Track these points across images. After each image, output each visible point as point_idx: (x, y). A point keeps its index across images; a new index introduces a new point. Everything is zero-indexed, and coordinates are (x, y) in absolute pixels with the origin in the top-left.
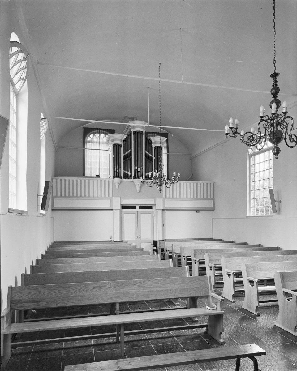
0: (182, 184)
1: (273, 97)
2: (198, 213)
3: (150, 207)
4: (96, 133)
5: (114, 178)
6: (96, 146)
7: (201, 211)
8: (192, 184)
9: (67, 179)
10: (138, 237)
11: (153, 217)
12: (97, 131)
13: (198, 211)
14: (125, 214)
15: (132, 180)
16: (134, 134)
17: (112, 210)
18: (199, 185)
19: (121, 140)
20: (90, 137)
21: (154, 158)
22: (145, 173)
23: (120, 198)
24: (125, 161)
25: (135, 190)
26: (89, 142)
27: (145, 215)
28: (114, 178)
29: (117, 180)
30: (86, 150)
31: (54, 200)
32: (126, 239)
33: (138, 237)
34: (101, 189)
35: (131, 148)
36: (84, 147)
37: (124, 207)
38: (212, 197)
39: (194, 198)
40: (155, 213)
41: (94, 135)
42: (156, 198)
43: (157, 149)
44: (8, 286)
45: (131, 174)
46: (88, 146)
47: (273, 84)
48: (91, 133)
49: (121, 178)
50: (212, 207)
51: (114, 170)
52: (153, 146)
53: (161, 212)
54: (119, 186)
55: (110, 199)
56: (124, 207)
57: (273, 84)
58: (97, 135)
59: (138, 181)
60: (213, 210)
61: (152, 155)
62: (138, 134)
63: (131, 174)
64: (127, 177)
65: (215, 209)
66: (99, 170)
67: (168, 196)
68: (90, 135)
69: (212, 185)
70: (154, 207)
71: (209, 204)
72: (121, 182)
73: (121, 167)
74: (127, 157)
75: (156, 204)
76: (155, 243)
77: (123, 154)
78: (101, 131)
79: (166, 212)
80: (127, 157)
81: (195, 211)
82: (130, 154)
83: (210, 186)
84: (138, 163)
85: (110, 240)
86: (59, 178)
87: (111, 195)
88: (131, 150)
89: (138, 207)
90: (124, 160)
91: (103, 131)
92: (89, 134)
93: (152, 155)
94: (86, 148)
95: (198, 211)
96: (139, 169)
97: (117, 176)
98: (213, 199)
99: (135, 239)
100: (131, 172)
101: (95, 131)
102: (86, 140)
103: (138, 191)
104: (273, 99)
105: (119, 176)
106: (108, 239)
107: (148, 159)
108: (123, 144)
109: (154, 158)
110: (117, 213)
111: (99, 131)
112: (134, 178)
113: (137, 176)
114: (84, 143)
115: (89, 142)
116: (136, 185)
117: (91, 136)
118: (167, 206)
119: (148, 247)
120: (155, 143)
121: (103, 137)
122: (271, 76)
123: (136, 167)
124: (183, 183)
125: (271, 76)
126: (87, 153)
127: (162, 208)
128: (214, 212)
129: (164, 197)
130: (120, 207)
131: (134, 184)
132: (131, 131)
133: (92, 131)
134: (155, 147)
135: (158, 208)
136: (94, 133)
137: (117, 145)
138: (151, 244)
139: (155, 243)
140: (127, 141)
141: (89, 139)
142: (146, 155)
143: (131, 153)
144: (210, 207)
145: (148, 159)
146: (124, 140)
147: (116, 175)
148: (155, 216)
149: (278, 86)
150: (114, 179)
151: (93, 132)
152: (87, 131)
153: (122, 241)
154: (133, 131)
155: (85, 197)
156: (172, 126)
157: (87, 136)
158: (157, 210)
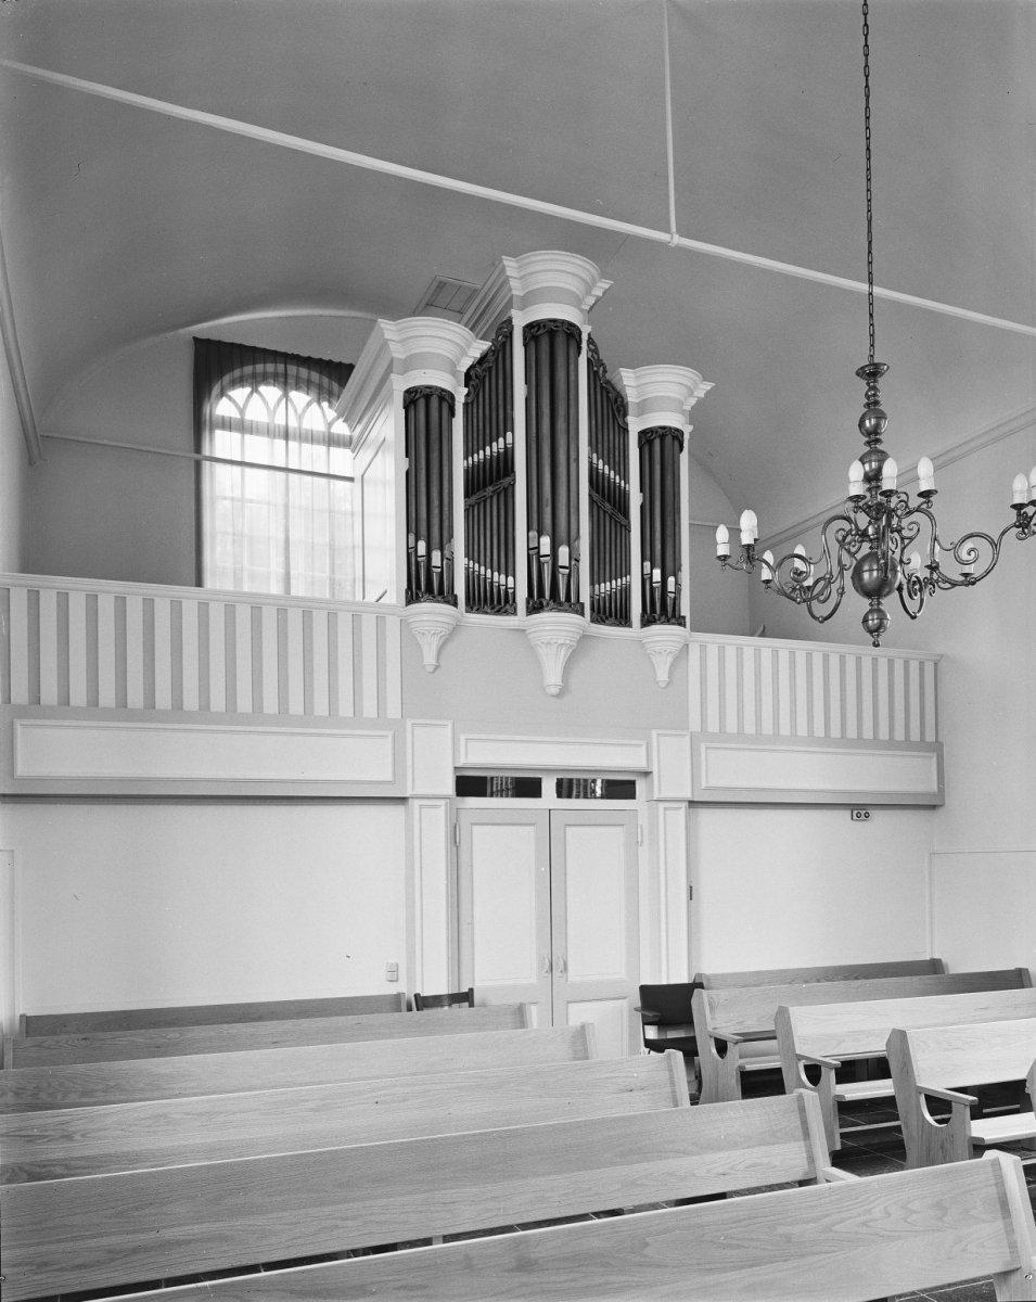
0: (713, 651)
1: (868, 443)
2: (860, 826)
3: (620, 789)
4: (264, 378)
5: (412, 596)
6: (258, 448)
7: (874, 813)
8: (784, 656)
9: (108, 590)
10: (553, 966)
11: (633, 845)
12: (270, 367)
13: (860, 810)
14: (475, 828)
15: (520, 618)
16: (525, 345)
17: (403, 800)
18: (821, 661)
19: (452, 369)
20: (230, 398)
21: (635, 500)
22: (592, 583)
23: (448, 731)
24: (473, 499)
25: (543, 679)
26: (227, 425)
27: (594, 836)
28: (412, 596)
29: (431, 613)
30: (206, 465)
31: (19, 730)
32: (481, 980)
33: (553, 966)
34: (776, 691)
35: (508, 425)
36: (198, 448)
37: (470, 785)
38: (930, 738)
39: (827, 740)
40: (643, 820)
41: (255, 390)
42: (654, 733)
43: (657, 442)
45: (511, 584)
46: (222, 443)
48: (237, 373)
49: (455, 604)
50: (934, 788)
51: (411, 553)
52: (635, 425)
53: (682, 812)
55: (390, 734)
56: (470, 785)
58: (271, 392)
59: (556, 626)
60: (934, 807)
61: (626, 478)
62: (552, 339)
64: (488, 600)
65: (951, 800)
66: (282, 559)
67: (713, 727)
68: (234, 384)
69: (929, 667)
70: (640, 787)
71: (912, 775)
72: (456, 628)
74: (490, 480)
75: (655, 770)
76: (668, 1009)
77: (466, 458)
78: (292, 369)
79: (705, 815)
80: (490, 480)
81: (847, 813)
82: (505, 462)
83: (843, 671)
84: (550, 517)
85: (392, 990)
86: (50, 587)
87: (393, 711)
88: (509, 440)
89: (548, 787)
90: (467, 495)
91: (304, 372)
92: (227, 378)
93: (627, 481)
94: (206, 452)
95: (860, 810)
97: (429, 589)
98: (937, 748)
99: (534, 980)
100: (509, 570)
101: (260, 367)
102: (207, 409)
104: (868, 449)
105: (441, 592)
106: (375, 985)
107: (609, 500)
108: (461, 394)
109: (635, 500)
110: (433, 823)
111: (281, 367)
112: (534, 608)
113: (548, 595)
114: (199, 425)
115: (227, 425)
116: (542, 651)
117: (240, 393)
118: (713, 783)
119: (616, 1026)
120: (643, 407)
122: (861, 373)
123: (546, 541)
124: (722, 649)
125: (861, 373)
127: (688, 795)
128: (940, 811)
129: (695, 726)
130: (449, 787)
131: (531, 649)
132: (510, 321)
133: (242, 365)
134: (646, 437)
135: (666, 794)
136: (255, 381)
137: (428, 397)
138: (624, 1003)
139: (668, 1009)
140: (487, 376)
141: (223, 408)
142: (596, 479)
143: (507, 457)
144: (921, 788)
145: (609, 500)
146: (467, 375)
147: (423, 584)
148: (646, 842)
150: (415, 607)
151: (248, 369)
152: (218, 363)
153: (466, 997)
154: (520, 320)
155: (231, 715)
156: (825, 271)
157: (216, 390)
158: (662, 806)
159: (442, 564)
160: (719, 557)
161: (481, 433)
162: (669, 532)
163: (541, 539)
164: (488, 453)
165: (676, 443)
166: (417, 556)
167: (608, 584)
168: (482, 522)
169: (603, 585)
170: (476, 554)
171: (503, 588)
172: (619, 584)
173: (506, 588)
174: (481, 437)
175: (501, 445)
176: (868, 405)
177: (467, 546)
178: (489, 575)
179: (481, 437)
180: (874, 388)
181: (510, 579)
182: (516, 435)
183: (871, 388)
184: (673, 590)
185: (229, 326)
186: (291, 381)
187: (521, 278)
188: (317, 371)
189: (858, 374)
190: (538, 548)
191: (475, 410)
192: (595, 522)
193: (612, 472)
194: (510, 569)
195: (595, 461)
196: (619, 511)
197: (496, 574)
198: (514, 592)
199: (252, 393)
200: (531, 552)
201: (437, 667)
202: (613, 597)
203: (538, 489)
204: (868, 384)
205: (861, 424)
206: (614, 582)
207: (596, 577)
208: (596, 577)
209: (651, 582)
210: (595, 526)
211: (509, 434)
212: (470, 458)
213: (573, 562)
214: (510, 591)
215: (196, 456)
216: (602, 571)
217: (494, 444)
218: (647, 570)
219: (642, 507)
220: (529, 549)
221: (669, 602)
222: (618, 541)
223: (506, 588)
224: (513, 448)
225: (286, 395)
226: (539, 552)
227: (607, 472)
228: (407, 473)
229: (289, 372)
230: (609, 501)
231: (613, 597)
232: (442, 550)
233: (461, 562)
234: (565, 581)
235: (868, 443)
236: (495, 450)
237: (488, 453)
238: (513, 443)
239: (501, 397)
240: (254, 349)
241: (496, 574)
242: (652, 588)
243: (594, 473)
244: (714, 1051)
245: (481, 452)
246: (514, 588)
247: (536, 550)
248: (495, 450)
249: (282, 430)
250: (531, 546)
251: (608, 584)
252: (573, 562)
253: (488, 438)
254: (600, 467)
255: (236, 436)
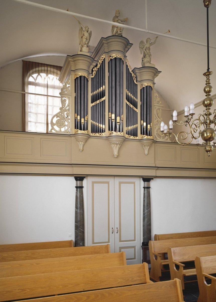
1: (206, 96)
4: (42, 71)
12: (43, 68)
20: (33, 77)
26: (31, 83)
41: (39, 74)
44: (212, 115)
45: (104, 127)
46: (31, 89)
47: (206, 83)
48: (34, 70)
54: (85, 146)
57: (206, 83)
58: (43, 75)
61: (137, 97)
63: (104, 127)
73: (87, 114)
78: (49, 69)
88: (104, 88)
91: (52, 69)
92: (31, 71)
94: (26, 92)
96: (118, 118)
100: (103, 123)
101: (40, 68)
103: (116, 156)
104: (206, 97)
111: (46, 68)
114: (24, 85)
115: (31, 83)
117: (35, 75)
121: (52, 79)
122: (204, 74)
123: (113, 116)
125: (204, 74)
126: (30, 99)
133: (36, 68)
136: (39, 72)
141: (31, 79)
149: (210, 85)
151: (37, 69)
152: (29, 67)
159: (84, 122)
160: (161, 131)
161: (96, 86)
162: (148, 112)
163: (112, 115)
164: (98, 91)
165: (151, 88)
166: (77, 120)
167: (131, 127)
168: (96, 110)
169: (130, 127)
170: (94, 119)
171: (102, 128)
172: (134, 126)
173: (103, 128)
174: (96, 87)
175: (102, 89)
176: (206, 84)
177: (92, 117)
178: (98, 125)
179: (96, 87)
180: (209, 79)
181: (104, 126)
182: (106, 86)
183: (207, 79)
184: (149, 128)
185: (33, 58)
186: (49, 72)
187: (107, 43)
188: (52, 68)
189: (204, 75)
190: (111, 117)
191: (94, 80)
192: (128, 110)
193: (133, 96)
194: (104, 123)
195: (128, 93)
196: (135, 107)
197: (100, 124)
198: (105, 129)
199: (38, 76)
200: (109, 118)
201: (83, 150)
202: (133, 130)
203: (109, 87)
204: (207, 78)
205: (205, 90)
206: (133, 126)
207: (128, 125)
208: (128, 125)
209: (143, 126)
210: (128, 111)
211: (104, 86)
212: (93, 93)
213: (121, 121)
214: (104, 129)
215: (23, 92)
216: (129, 124)
217: (100, 89)
218: (142, 123)
219: (141, 106)
220: (109, 118)
221: (148, 132)
222: (134, 115)
223: (103, 128)
224: (105, 90)
225: (47, 75)
226: (111, 118)
227: (131, 96)
228: (75, 97)
229: (48, 69)
230: (132, 104)
231: (133, 130)
232: (84, 118)
233: (90, 121)
234: (119, 126)
235: (206, 96)
236: (100, 90)
237: (98, 91)
238: (105, 89)
239: (102, 76)
240: (38, 63)
241: (100, 124)
242: (143, 128)
243: (128, 96)
244: (175, 268)
245: (96, 91)
246: (105, 128)
247: (111, 118)
248: (100, 90)
249: (46, 85)
250: (109, 117)
251: (131, 127)
252: (121, 121)
253: (98, 87)
254: (129, 94)
255: (34, 87)
